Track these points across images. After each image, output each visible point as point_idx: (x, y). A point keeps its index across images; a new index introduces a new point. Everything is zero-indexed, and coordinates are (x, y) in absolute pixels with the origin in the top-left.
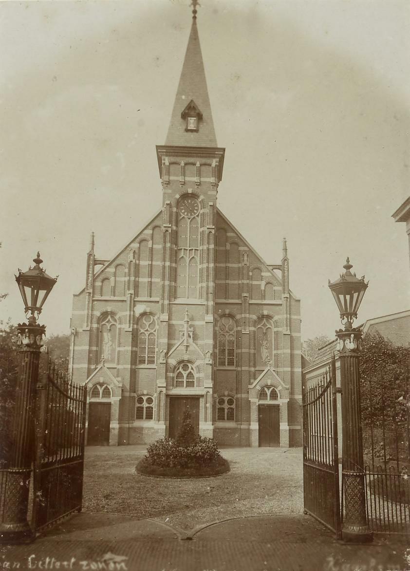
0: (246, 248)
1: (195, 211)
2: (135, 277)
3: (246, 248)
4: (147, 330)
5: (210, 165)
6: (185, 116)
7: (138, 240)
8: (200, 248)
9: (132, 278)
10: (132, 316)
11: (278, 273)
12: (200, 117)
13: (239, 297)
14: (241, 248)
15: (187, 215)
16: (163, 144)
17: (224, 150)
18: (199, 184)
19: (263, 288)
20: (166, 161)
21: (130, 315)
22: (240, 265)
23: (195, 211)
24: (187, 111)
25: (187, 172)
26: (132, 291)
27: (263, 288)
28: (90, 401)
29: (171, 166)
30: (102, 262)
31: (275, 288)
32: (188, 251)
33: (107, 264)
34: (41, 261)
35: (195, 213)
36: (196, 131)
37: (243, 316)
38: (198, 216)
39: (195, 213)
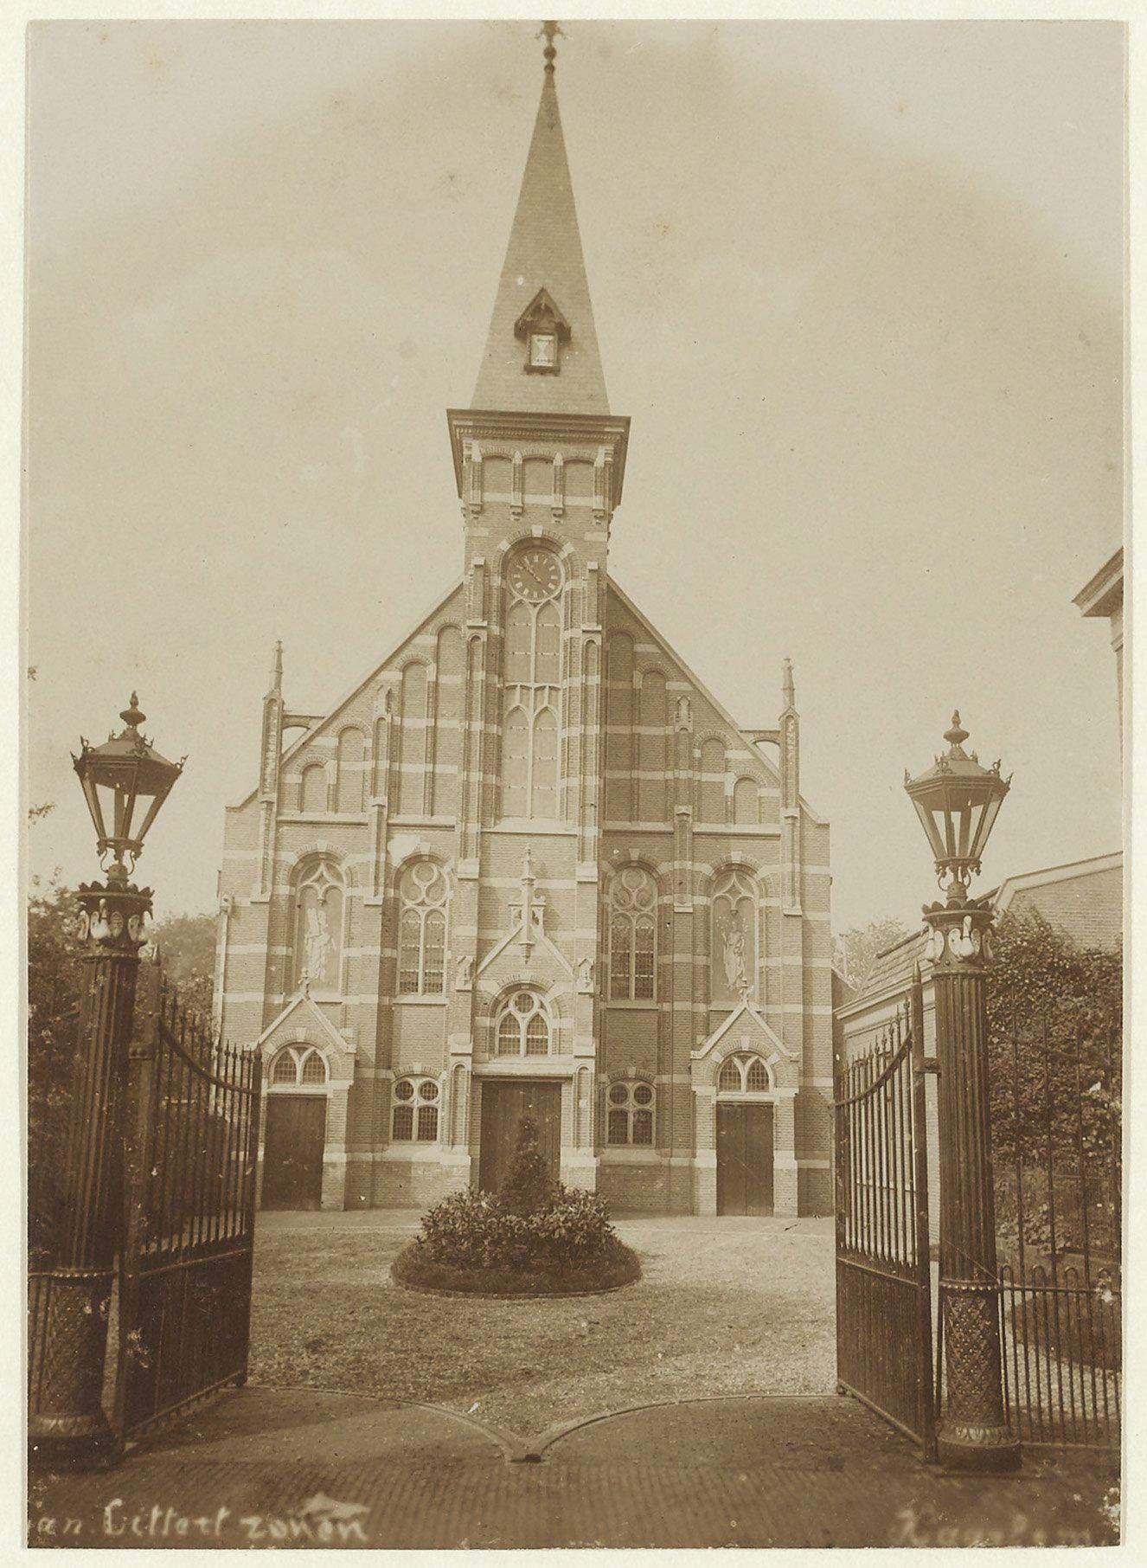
0: (686, 686)
1: (551, 586)
2: (392, 759)
3: (686, 686)
4: (422, 903)
5: (590, 462)
6: (523, 331)
7: (398, 662)
8: (564, 684)
9: (384, 764)
10: (382, 866)
11: (771, 752)
12: (563, 335)
13: (666, 815)
14: (672, 686)
15: (530, 595)
16: (466, 406)
17: (627, 422)
18: (561, 514)
19: (729, 791)
20: (475, 450)
21: (377, 862)
22: (669, 730)
23: (551, 586)
24: (529, 319)
25: (530, 482)
26: (382, 799)
27: (729, 791)
28: (270, 1090)
29: (489, 464)
30: (302, 721)
31: (763, 792)
32: (532, 691)
33: (315, 725)
34: (142, 718)
35: (550, 591)
36: (554, 371)
37: (677, 865)
38: (557, 598)
39: (550, 591)
